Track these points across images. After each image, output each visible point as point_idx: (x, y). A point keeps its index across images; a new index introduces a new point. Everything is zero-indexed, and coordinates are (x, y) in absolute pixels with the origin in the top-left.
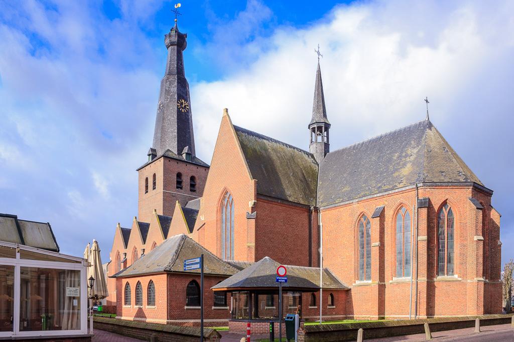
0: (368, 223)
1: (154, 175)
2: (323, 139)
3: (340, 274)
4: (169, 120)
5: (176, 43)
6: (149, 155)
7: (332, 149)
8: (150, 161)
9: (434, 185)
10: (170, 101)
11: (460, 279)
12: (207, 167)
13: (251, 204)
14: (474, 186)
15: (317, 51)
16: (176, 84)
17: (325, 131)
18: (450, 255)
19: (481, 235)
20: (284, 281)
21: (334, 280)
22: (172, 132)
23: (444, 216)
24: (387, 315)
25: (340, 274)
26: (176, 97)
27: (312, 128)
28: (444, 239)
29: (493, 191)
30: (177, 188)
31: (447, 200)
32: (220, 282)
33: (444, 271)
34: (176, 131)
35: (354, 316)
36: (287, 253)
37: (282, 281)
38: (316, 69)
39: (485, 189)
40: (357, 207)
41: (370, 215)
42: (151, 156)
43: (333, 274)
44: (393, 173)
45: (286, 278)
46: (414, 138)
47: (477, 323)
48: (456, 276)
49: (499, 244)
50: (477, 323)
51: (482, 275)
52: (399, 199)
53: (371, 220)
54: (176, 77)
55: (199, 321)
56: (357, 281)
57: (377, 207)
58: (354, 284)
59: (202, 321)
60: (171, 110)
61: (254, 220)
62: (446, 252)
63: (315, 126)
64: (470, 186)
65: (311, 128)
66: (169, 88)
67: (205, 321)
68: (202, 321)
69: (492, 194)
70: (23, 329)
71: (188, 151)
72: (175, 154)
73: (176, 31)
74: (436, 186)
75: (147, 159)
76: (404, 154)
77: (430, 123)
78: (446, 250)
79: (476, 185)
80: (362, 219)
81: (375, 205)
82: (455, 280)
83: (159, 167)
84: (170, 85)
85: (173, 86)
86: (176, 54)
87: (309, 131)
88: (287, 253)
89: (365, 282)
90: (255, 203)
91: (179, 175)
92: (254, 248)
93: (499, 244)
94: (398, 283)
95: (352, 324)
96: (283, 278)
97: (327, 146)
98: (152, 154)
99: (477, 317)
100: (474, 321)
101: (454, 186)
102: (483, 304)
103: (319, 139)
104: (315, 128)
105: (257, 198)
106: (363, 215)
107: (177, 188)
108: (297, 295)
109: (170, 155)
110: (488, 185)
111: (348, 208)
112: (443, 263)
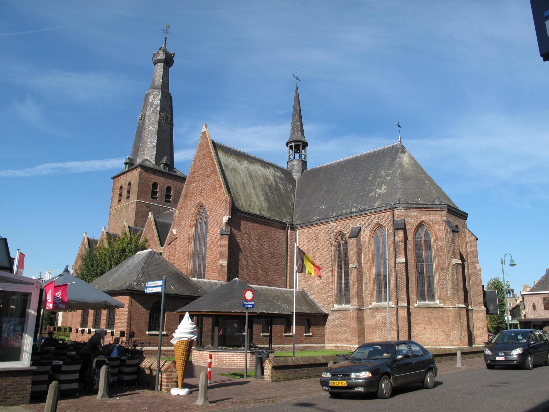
0: (346, 242)
1: (130, 184)
2: (300, 157)
3: (318, 297)
4: (150, 130)
5: (163, 61)
6: (126, 164)
7: (309, 167)
8: (127, 169)
9: (408, 207)
10: (153, 113)
11: (442, 305)
12: (183, 179)
13: (225, 219)
14: (448, 209)
15: (295, 76)
16: (160, 97)
17: (302, 150)
18: (429, 279)
19: (459, 258)
20: (251, 306)
21: (311, 304)
22: (152, 142)
23: (421, 238)
24: (275, 344)
25: (318, 297)
26: (159, 109)
27: (290, 146)
28: (423, 262)
29: (467, 214)
30: (152, 197)
31: (423, 221)
32: (187, 304)
33: (425, 296)
34: (156, 141)
35: (326, 345)
36: (261, 272)
37: (249, 306)
38: (295, 88)
39: (459, 212)
40: (335, 226)
41: (347, 234)
42: (127, 166)
43: (310, 297)
44: (369, 192)
45: (253, 303)
46: (388, 160)
47: (459, 354)
48: (438, 302)
49: (478, 268)
50: (459, 354)
51: (463, 302)
52: (375, 218)
53: (348, 239)
54: (160, 91)
55: (157, 348)
56: (335, 305)
57: (354, 227)
58: (332, 309)
59: (294, 346)
60: (153, 121)
61: (228, 236)
62: (425, 276)
63: (293, 144)
64: (445, 208)
65: (289, 145)
66: (153, 100)
67: (163, 348)
68: (294, 346)
69: (467, 217)
70: (520, 328)
71: (166, 161)
72: (153, 164)
73: (164, 51)
74: (411, 208)
75: (124, 168)
76: (378, 176)
77: (402, 146)
78: (425, 273)
79: (450, 208)
80: (339, 238)
81: (351, 225)
82: (436, 306)
83: (134, 176)
84: (154, 98)
85: (157, 99)
86: (162, 70)
87: (287, 149)
88: (261, 272)
89: (344, 306)
90: (229, 218)
91: (155, 185)
92: (226, 266)
93: (478, 268)
94: (377, 308)
95: (323, 357)
96: (250, 303)
97: (304, 163)
98: (129, 163)
99: (457, 349)
100: (455, 354)
101: (428, 208)
102: (467, 333)
103: (297, 156)
104: (293, 145)
105: (232, 213)
106: (341, 234)
107: (152, 197)
108: (269, 319)
109: (147, 164)
110: (462, 208)
111: (325, 226)
112: (423, 287)
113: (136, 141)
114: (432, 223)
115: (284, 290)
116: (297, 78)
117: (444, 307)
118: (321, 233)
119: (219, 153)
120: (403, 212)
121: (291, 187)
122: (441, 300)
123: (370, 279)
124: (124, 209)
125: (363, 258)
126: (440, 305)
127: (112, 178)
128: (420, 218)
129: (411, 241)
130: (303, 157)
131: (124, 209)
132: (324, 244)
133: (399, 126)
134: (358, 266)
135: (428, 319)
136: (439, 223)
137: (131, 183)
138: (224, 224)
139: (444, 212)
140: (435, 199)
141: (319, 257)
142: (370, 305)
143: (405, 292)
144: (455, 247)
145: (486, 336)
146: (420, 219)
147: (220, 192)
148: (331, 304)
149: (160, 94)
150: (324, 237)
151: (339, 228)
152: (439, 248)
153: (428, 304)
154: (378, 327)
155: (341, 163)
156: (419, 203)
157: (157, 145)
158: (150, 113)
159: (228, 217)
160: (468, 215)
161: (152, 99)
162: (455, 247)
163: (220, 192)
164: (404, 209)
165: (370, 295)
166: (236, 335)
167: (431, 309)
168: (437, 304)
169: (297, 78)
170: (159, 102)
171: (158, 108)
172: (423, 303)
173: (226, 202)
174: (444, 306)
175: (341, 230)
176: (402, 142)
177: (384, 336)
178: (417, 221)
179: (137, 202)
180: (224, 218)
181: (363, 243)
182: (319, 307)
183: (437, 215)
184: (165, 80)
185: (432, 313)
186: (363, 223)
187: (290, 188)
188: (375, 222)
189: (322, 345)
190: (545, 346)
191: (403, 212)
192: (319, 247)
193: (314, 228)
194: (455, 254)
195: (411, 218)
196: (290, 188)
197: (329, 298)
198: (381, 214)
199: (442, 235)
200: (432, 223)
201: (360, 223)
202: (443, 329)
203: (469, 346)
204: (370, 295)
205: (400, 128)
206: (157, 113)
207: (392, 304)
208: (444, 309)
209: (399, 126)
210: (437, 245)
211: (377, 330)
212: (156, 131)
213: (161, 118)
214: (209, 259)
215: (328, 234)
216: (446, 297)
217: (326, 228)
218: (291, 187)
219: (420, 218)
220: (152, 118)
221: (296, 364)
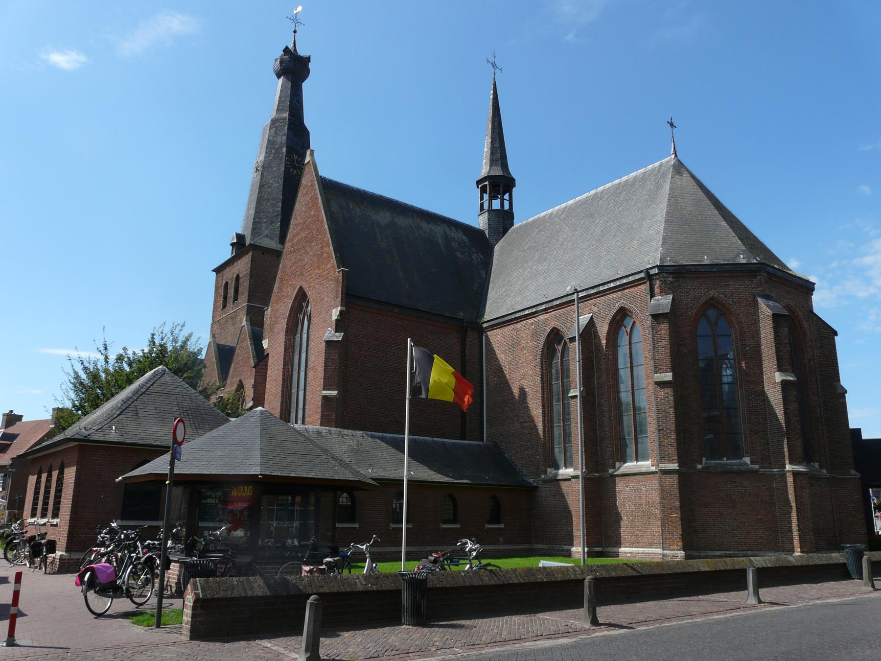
11: (756, 467)
13: (335, 313)
26: (284, 150)
38: (492, 82)
65: (480, 186)
113: (250, 206)
114: (730, 302)
115: (454, 443)
116: (494, 65)
117: (761, 470)
118: (523, 335)
119: (621, 313)
120: (669, 282)
121: (480, 258)
122: (754, 457)
123: (609, 418)
124: (229, 320)
125: (597, 378)
126: (753, 466)
127: (213, 271)
128: (707, 292)
129: (688, 339)
130: (507, 204)
131: (229, 320)
132: (528, 354)
133: (672, 125)
134: (586, 392)
135: (727, 496)
136: (747, 300)
137: (240, 276)
138: (334, 323)
139: (757, 279)
140: (738, 255)
141: (521, 379)
142: (610, 469)
143: (673, 441)
144: (781, 348)
145: (862, 532)
146: (705, 294)
147: (329, 266)
148: (542, 468)
149: (287, 126)
150: (529, 341)
151: (553, 324)
152: (748, 350)
153: (727, 465)
154: (627, 512)
155: (568, 209)
156: (703, 263)
157: (282, 212)
158: (270, 159)
159: (339, 308)
160: (815, 286)
161: (273, 135)
162: (781, 348)
163: (329, 266)
164: (671, 276)
165: (610, 449)
166: (486, 528)
167: (732, 475)
168: (746, 464)
169: (494, 65)
170: (285, 138)
171: (283, 148)
172: (715, 463)
173: (337, 281)
174: (759, 468)
175: (557, 327)
176: (678, 155)
177: (638, 530)
178: (699, 298)
179: (248, 305)
180: (334, 310)
181: (595, 348)
182: (521, 474)
183: (742, 285)
184: (294, 102)
185: (735, 482)
186: (595, 309)
187: (479, 259)
188: (617, 305)
189: (393, 549)
190: (322, 577)
191: (669, 282)
192: (520, 362)
193: (512, 326)
194: (781, 361)
195: (687, 293)
196: (479, 259)
197: (538, 457)
198: (627, 290)
199: (752, 325)
200: (730, 302)
201: (591, 309)
202: (759, 517)
203: (801, 552)
204: (610, 449)
205: (674, 129)
206: (282, 157)
207: (652, 466)
208: (761, 474)
209: (672, 125)
210: (744, 345)
211: (625, 518)
212: (281, 188)
213: (288, 165)
214: (311, 388)
215: (535, 334)
216: (765, 450)
217: (532, 324)
218: (480, 258)
219: (707, 292)
220: (275, 167)
221: (814, 563)
